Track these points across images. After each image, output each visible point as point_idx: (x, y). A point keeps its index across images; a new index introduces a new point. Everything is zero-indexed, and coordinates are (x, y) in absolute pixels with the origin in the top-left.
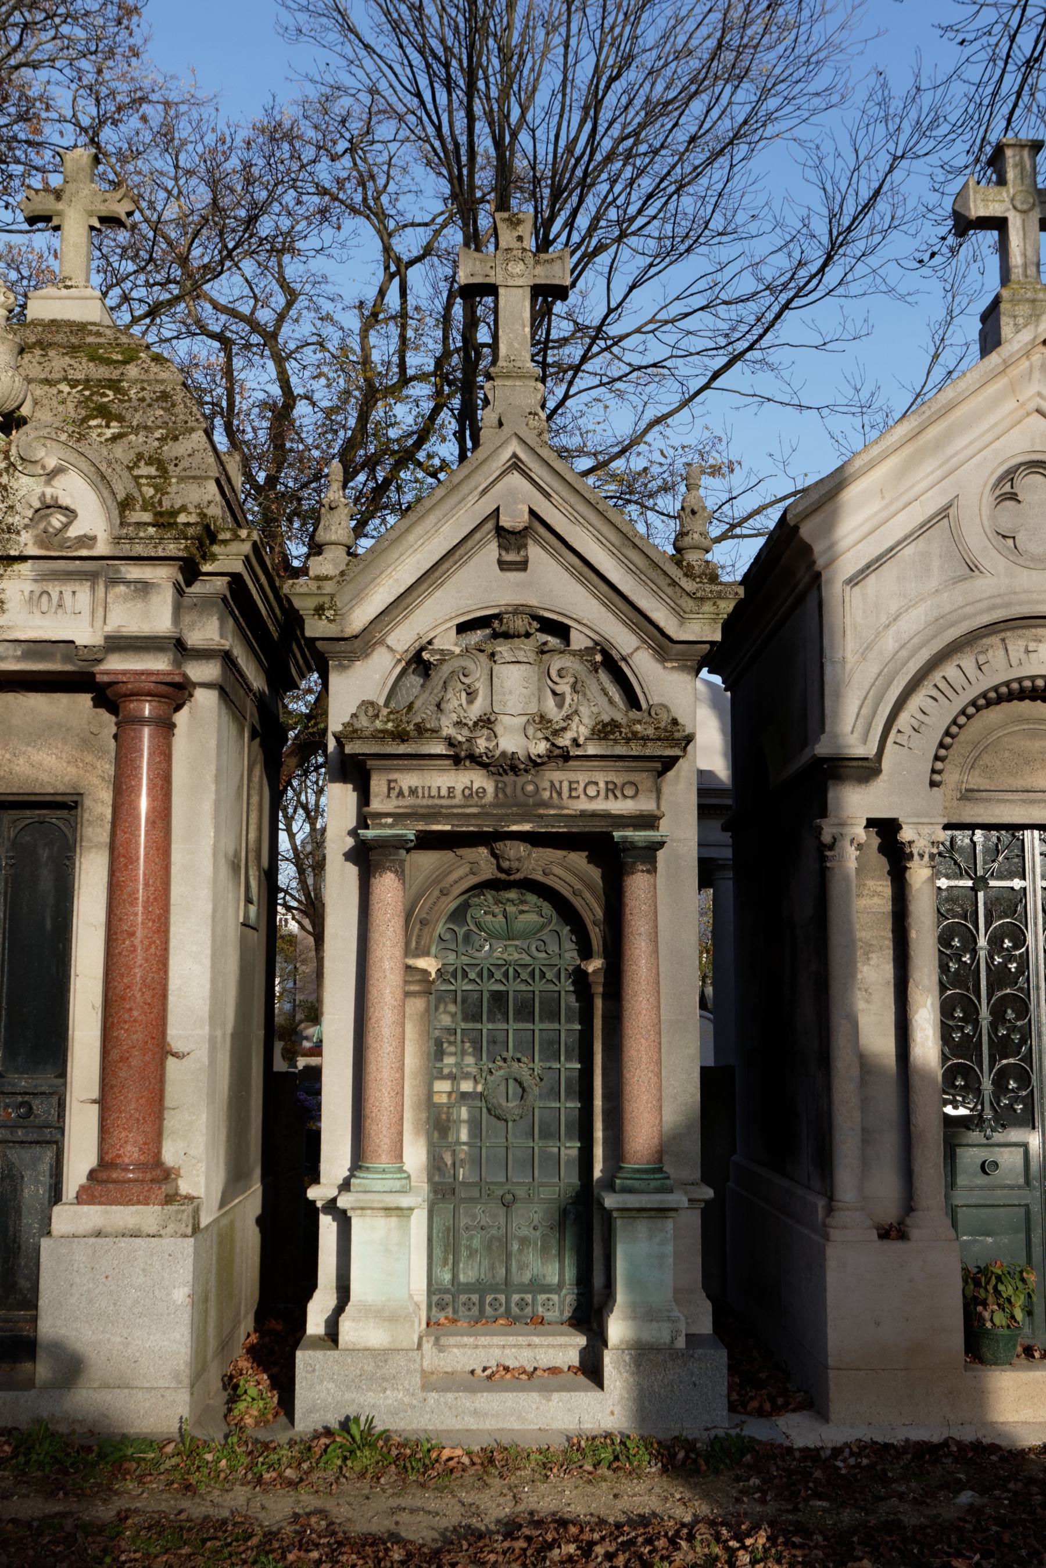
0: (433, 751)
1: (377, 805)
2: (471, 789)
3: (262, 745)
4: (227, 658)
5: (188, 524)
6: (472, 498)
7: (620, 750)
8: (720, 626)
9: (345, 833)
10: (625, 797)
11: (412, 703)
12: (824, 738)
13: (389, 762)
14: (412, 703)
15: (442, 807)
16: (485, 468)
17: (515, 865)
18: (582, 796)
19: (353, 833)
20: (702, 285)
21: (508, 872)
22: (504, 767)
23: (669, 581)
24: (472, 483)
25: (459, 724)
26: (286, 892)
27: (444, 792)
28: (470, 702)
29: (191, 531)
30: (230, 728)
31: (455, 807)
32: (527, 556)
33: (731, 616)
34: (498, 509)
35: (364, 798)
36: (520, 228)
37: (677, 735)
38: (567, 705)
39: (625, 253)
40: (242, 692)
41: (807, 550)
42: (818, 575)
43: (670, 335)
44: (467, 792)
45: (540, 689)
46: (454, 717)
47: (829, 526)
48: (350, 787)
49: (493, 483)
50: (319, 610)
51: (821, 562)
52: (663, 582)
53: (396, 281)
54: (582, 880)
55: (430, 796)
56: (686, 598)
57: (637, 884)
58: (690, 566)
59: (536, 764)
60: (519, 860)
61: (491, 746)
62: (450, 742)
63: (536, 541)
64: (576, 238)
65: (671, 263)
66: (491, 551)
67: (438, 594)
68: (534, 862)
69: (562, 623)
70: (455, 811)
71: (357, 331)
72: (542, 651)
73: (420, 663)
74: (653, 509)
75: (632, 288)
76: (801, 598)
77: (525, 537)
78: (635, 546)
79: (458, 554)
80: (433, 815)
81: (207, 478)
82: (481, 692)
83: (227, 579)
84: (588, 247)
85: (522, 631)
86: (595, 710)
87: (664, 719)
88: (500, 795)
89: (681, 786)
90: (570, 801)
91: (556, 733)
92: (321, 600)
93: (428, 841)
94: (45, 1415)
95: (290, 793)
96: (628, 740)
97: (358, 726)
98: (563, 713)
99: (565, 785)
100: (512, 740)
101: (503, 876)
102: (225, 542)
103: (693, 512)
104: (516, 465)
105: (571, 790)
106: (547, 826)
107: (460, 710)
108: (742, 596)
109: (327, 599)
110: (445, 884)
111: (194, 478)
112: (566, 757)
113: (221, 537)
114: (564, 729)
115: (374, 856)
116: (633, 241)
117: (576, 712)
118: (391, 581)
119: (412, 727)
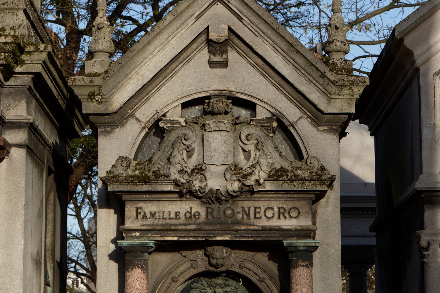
0: (165, 189)
1: (129, 224)
2: (190, 213)
3: (56, 179)
4: (32, 128)
5: (6, 43)
6: (191, 21)
7: (287, 187)
9: (109, 241)
10: (291, 217)
11: (151, 158)
12: (422, 177)
13: (137, 196)
15: (171, 225)
17: (220, 262)
18: (263, 217)
19: (114, 241)
21: (216, 266)
23: (320, 74)
24: (191, 11)
25: (182, 171)
26: (77, 263)
27: (173, 215)
28: (189, 157)
29: (8, 48)
30: (34, 171)
31: (180, 225)
32: (227, 58)
34: (208, 27)
35: (121, 220)
37: (324, 177)
40: (41, 146)
41: (409, 53)
42: (418, 70)
44: (188, 215)
45: (234, 148)
46: (179, 167)
47: (427, 36)
50: (91, 96)
51: (419, 61)
52: (316, 75)
54: (265, 271)
55: (164, 218)
57: (300, 275)
58: (334, 63)
59: (232, 197)
60: (223, 258)
62: (176, 183)
66: (204, 55)
68: (233, 260)
69: (251, 102)
72: (236, 122)
73: (158, 129)
76: (409, 83)
77: (226, 45)
78: (298, 51)
80: (166, 230)
81: (18, 9)
82: (196, 150)
83: (31, 76)
85: (222, 110)
86: (270, 161)
88: (210, 217)
89: (330, 209)
91: (245, 176)
92: (92, 89)
93: (162, 247)
95: (79, 187)
96: (292, 181)
97: (116, 173)
98: (250, 163)
99: (252, 209)
100: (215, 182)
101: (213, 269)
102: (30, 53)
103: (337, 28)
105: (255, 213)
106: (240, 237)
107: (182, 162)
109: (96, 89)
110: (175, 274)
111: (10, 9)
112: (252, 192)
113: (27, 49)
114: (250, 174)
115: (128, 257)
117: (258, 163)
118: (138, 76)
119: (151, 173)
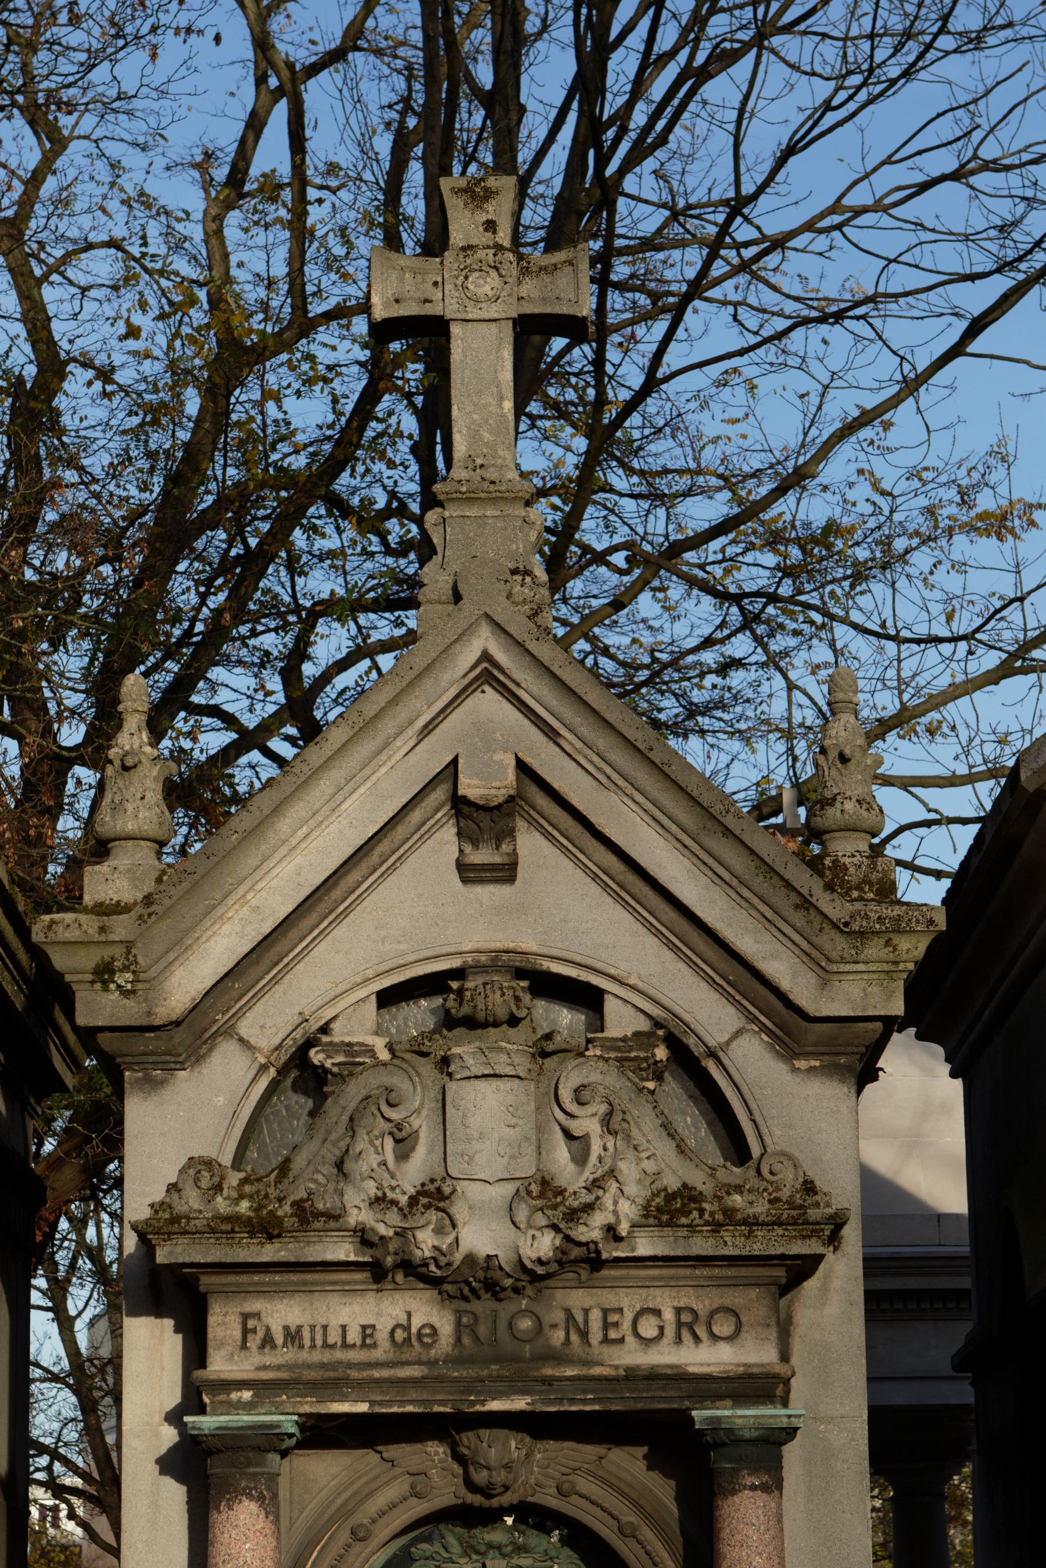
1: (220, 1364)
2: (407, 1328)
6: (404, 743)
7: (702, 1245)
8: (900, 986)
9: (159, 1417)
10: (715, 1338)
11: (287, 1161)
13: (244, 1278)
14: (287, 1161)
15: (350, 1365)
16: (428, 683)
17: (500, 1477)
18: (630, 1339)
19: (174, 1417)
20: (946, 129)
21: (486, 1491)
22: (470, 1284)
24: (402, 713)
25: (380, 1202)
26: (55, 1455)
27: (354, 1336)
28: (403, 1156)
32: (514, 853)
33: (923, 965)
34: (455, 762)
35: (196, 1353)
36: (491, 206)
37: (814, 1214)
38: (593, 1158)
39: (774, 73)
43: (883, 236)
44: (400, 1335)
45: (539, 1129)
46: (371, 1188)
48: (169, 1323)
49: (444, 712)
52: (784, 902)
53: (281, 110)
54: (636, 1504)
55: (326, 1345)
56: (830, 932)
59: (535, 1278)
60: (507, 1467)
61: (445, 1243)
62: (364, 1238)
63: (532, 822)
64: (667, 37)
65: (871, 101)
66: (445, 843)
67: (339, 932)
68: (541, 1470)
70: (376, 1374)
71: (198, 215)
72: (544, 1050)
73: (305, 1072)
74: (845, 621)
75: (790, 151)
77: (511, 815)
78: (727, 832)
79: (377, 852)
82: (423, 1135)
84: (692, 57)
85: (502, 1014)
86: (650, 1166)
87: (789, 1180)
88: (466, 1341)
89: (833, 1309)
90: (606, 1349)
91: (574, 1215)
92: (107, 953)
93: (322, 1433)
94: (761, 878)
95: (64, 1224)
96: (716, 1227)
97: (181, 1208)
98: (587, 1175)
99: (596, 1315)
100: (482, 1234)
101: (477, 1500)
103: (844, 759)
104: (488, 674)
105: (606, 1326)
106: (559, 1401)
108: (943, 926)
109: (118, 951)
110: (361, 1517)
114: (589, 1208)
115: (216, 1468)
116: (786, 44)
117: (612, 1173)
118: (245, 912)
119: (287, 1208)
